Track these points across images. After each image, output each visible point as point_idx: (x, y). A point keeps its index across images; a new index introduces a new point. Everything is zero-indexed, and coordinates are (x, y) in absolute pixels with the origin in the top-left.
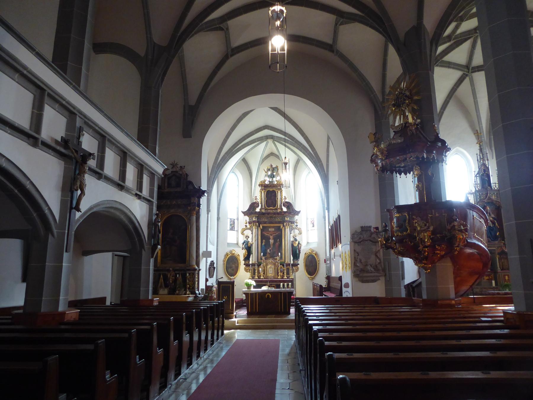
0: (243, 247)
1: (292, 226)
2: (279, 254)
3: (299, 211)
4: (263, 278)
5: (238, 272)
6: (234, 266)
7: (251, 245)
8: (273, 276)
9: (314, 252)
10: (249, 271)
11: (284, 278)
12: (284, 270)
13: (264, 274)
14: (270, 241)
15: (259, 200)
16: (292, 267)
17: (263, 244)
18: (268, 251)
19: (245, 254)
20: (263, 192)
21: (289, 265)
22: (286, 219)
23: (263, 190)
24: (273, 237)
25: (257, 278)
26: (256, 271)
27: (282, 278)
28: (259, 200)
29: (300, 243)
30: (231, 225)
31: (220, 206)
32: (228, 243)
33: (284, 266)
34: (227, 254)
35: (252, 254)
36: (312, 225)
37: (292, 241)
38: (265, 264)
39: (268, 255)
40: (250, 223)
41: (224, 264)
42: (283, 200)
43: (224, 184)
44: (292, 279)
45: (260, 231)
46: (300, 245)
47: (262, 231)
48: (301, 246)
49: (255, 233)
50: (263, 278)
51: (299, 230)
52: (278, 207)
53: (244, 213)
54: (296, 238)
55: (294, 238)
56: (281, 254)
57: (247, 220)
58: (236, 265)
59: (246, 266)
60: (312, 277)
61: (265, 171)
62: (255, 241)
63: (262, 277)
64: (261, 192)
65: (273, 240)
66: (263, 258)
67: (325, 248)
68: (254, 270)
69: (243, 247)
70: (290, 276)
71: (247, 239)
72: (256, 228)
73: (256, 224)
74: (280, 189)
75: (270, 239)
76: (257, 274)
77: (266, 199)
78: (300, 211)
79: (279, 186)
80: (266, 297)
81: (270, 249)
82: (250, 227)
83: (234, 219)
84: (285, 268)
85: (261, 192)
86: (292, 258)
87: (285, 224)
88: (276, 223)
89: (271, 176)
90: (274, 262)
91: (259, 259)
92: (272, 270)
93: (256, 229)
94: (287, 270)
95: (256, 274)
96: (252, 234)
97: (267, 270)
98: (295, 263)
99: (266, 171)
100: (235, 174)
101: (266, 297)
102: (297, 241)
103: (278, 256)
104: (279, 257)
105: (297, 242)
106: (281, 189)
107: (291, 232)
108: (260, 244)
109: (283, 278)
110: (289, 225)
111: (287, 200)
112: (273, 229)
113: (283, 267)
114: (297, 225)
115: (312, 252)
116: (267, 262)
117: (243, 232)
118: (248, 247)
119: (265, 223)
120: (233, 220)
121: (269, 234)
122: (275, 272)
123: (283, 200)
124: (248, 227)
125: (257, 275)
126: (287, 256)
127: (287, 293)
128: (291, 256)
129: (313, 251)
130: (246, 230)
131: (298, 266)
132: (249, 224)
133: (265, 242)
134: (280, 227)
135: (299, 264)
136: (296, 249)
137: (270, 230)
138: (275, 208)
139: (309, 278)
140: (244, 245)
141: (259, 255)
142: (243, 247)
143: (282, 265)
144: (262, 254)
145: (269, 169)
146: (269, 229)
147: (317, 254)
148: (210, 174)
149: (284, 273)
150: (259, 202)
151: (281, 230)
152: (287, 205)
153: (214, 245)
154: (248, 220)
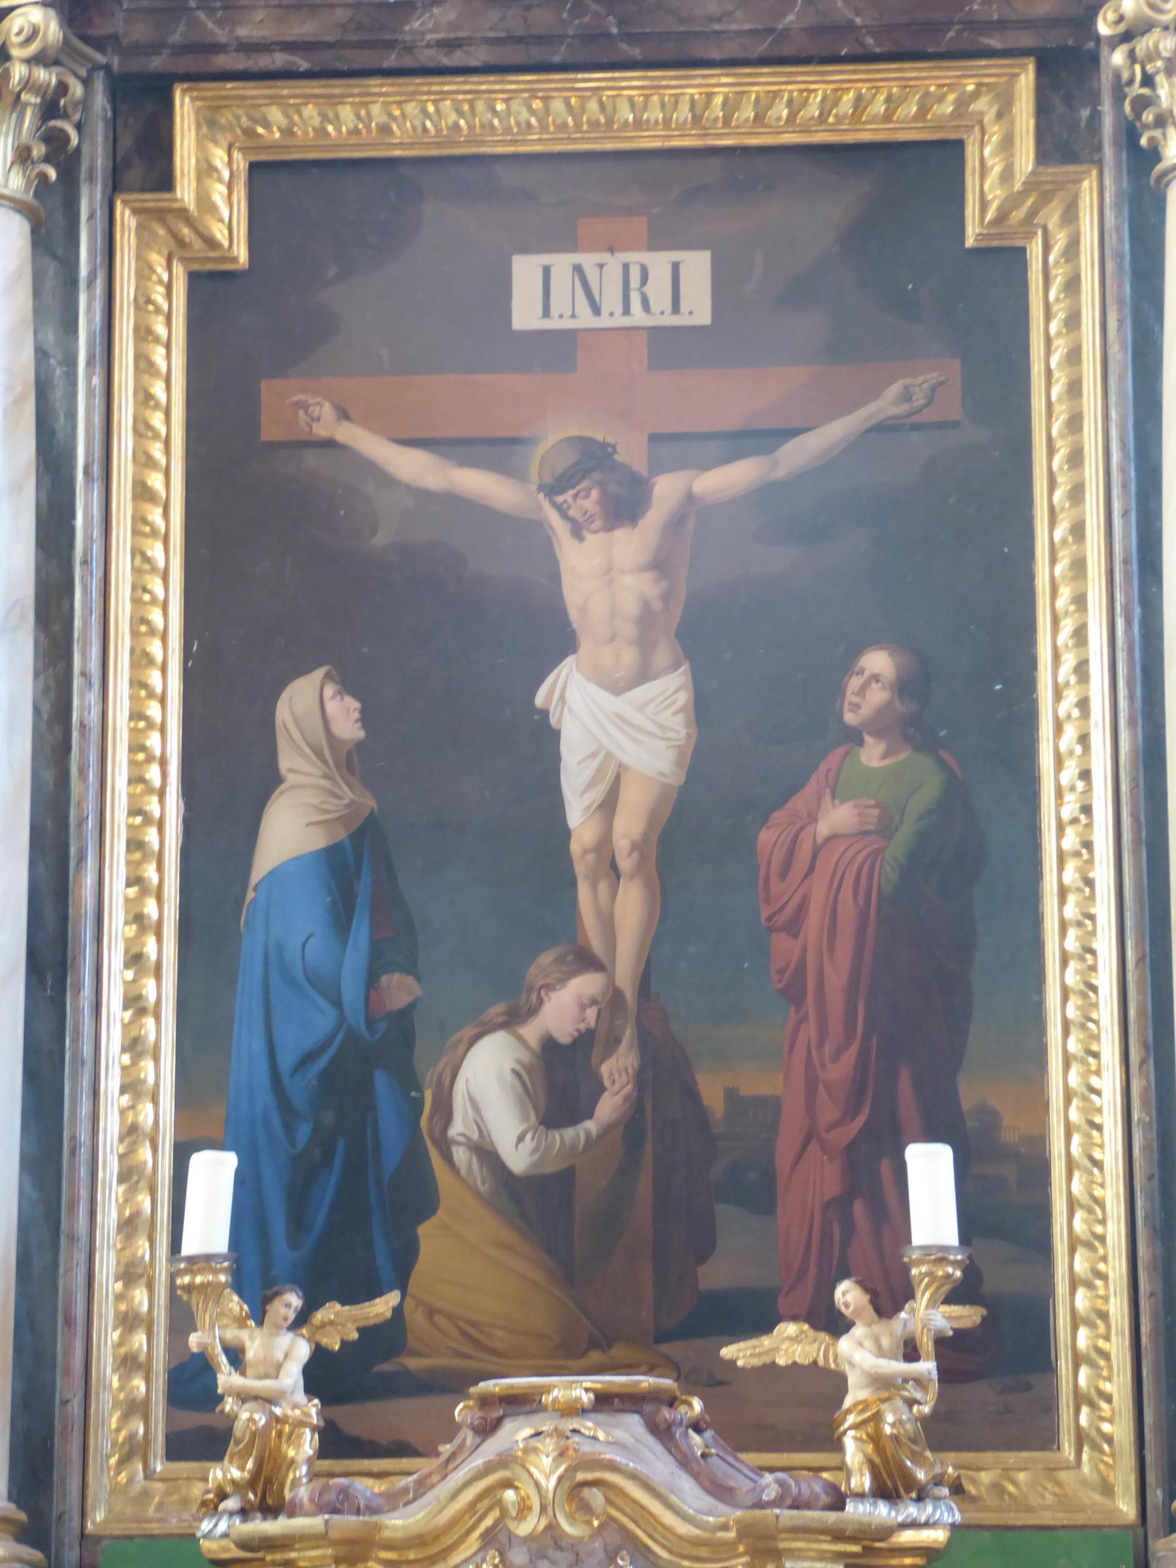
24: (659, 565)
116: (397, 1523)
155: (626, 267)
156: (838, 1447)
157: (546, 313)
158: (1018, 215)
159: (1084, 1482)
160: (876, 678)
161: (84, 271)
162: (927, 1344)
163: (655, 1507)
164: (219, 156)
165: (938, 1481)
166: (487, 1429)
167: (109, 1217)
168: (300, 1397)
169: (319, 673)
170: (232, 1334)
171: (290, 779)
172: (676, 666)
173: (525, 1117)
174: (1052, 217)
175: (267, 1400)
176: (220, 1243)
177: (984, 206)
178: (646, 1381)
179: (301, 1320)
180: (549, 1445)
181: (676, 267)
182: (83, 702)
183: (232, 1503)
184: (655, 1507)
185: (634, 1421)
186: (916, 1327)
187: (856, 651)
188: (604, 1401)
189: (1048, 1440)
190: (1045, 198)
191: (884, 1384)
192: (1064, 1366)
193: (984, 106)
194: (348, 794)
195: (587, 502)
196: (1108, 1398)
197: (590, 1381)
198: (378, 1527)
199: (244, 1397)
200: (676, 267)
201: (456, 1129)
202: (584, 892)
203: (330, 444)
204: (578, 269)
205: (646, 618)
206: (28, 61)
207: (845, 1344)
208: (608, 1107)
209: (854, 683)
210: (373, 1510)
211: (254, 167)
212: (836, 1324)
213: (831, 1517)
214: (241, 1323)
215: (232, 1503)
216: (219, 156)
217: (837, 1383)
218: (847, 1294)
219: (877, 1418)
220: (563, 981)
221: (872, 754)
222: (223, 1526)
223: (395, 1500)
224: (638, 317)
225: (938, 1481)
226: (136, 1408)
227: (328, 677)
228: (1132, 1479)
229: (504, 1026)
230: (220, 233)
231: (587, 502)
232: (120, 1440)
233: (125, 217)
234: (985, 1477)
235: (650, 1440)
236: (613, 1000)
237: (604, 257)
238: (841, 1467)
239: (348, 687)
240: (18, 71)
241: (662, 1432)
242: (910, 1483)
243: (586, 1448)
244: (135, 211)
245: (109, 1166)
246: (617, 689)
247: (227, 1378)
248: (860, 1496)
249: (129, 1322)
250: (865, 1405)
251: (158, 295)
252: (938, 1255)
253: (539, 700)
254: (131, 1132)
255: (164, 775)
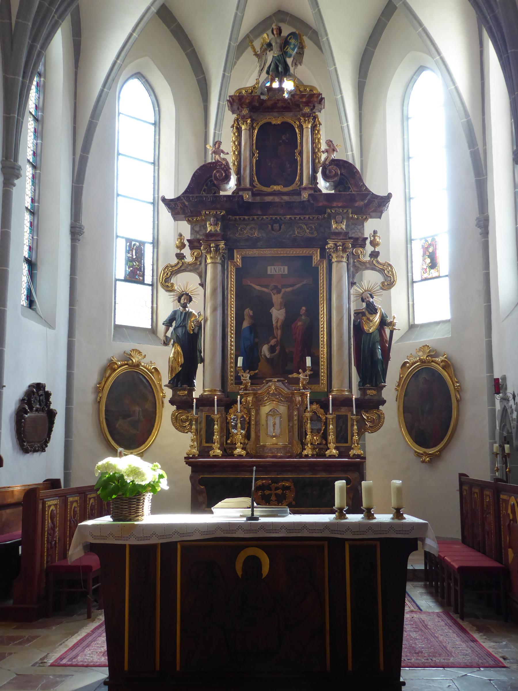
0: (169, 334)
1: (356, 256)
2: (308, 360)
3: (386, 195)
4: (244, 453)
5: (155, 432)
6: (137, 409)
7: (200, 327)
8: (285, 447)
9: (439, 360)
10: (191, 424)
11: (328, 453)
12: (326, 424)
13: (247, 436)
14: (271, 315)
15: (231, 159)
16: (358, 413)
17: (246, 324)
18: (265, 349)
19: (175, 359)
20: (243, 127)
21: (346, 402)
22: (334, 226)
23: (244, 118)
24: (282, 298)
25: (219, 452)
26: (216, 427)
27: (319, 456)
28: (231, 159)
29: (389, 320)
30: (129, 261)
31: (84, 186)
32: (118, 327)
33: (325, 406)
34: (111, 366)
35: (202, 361)
36: (428, 261)
37: (357, 313)
38: (250, 399)
39: (263, 366)
40: (194, 244)
41: (99, 402)
42: (323, 156)
43: (100, 95)
44: (358, 456)
45: (234, 277)
46: (387, 331)
47: (240, 273)
48: (392, 333)
49: (214, 278)
50: (244, 453)
51: (381, 271)
52: (302, 183)
53: (170, 204)
54: (371, 300)
55: (363, 300)
56: (316, 362)
57: (183, 235)
58: (148, 406)
59: (178, 408)
60: (431, 451)
61: (254, 51)
62: (214, 310)
63: (238, 451)
64: (239, 130)
65: (283, 311)
66: (246, 377)
67: (485, 340)
68: (210, 422)
69: (166, 337)
70: (350, 448)
71: (184, 306)
72: (219, 260)
73: (217, 246)
74: (309, 117)
75: (272, 305)
76: (221, 437)
77: (256, 155)
78: (389, 196)
79: (307, 104)
80: (240, 573)
81: (273, 342)
82: (196, 258)
83: (142, 243)
84: (329, 416)
85: (239, 130)
86: (355, 379)
87: (331, 244)
88: (295, 243)
89: (277, 67)
90: (285, 391)
91: (230, 382)
92: (277, 421)
93: (219, 267)
94: (337, 423)
95: (216, 437)
96: (203, 285)
97: (257, 423)
98: (367, 397)
99: (258, 49)
100: (147, 81)
101: (240, 573)
102: (376, 313)
103: (304, 370)
104: (308, 372)
105: (377, 319)
106: (315, 118)
107: (353, 278)
108: (234, 325)
109: (324, 456)
110: (344, 250)
111: (335, 156)
112: (284, 270)
113: (322, 411)
114: (378, 253)
115: (432, 356)
116: (259, 392)
117: (167, 280)
118: (187, 333)
119: (253, 244)
120: (138, 244)
121: (266, 286)
122: (291, 430)
123: (323, 156)
124: (189, 259)
125: (222, 445)
126: (341, 371)
127: (378, 543)
128: (354, 369)
129: (433, 354)
130: (178, 271)
131: (381, 407)
132: (192, 248)
133: (252, 317)
134: (310, 258)
135: (383, 402)
136: (374, 344)
137: (271, 270)
138: (290, 188)
139: (419, 455)
140: (171, 329)
141: (230, 360)
142: (166, 337)
143: (318, 402)
144: (240, 360)
145: (269, 45)
146: (269, 268)
147: (452, 364)
148: (18, 17)
149: (325, 436)
150: (231, 165)
151: (314, 273)
152: (336, 174)
153: (50, 324)
154: (187, 235)
155: (279, 268)
156: (299, 384)
157: (271, 272)
158: (318, 263)
159: (322, 388)
160: (304, 310)
161: (226, 268)
162: (308, 375)
163: (283, 391)
164: (238, 256)
165: (309, 388)
166: (267, 383)
167: (229, 362)
168: (249, 380)
169: (248, 308)
170: (242, 374)
171: (246, 319)
172: (284, 308)
173: (269, 352)
174: (321, 264)
175: (246, 380)
176: (241, 365)
177: (315, 262)
178: (282, 379)
179: (249, 373)
180: (273, 385)
181: (284, 268)
182: (226, 312)
183: (243, 389)
184: (283, 391)
185: (281, 383)
186: (307, 374)
187: (302, 307)
188: (278, 381)
189: (319, 384)
190: (320, 262)
191: (304, 379)
192: (320, 377)
193: (315, 252)
194: (251, 321)
195: (275, 291)
196: (324, 380)
197: (277, 379)
198: (257, 392)
199: (244, 380)
200: (284, 268)
201: (262, 354)
202: (275, 331)
203: (250, 285)
204: (274, 268)
205: (281, 303)
206: (222, 250)
207: (300, 375)
208: (277, 352)
209: (301, 310)
210: (257, 391)
211: (242, 257)
212: (299, 373)
213: (299, 391)
214: (243, 373)
215: (243, 389)
216: (238, 256)
217: (299, 379)
218: (300, 371)
219: (303, 382)
220: (272, 340)
221: (303, 317)
222: (242, 391)
223: (259, 389)
224: (280, 273)
225: (309, 388)
226: (232, 380)
227: (249, 309)
228: (327, 387)
229: (267, 344)
230: (238, 264)
231: (275, 291)
232: (510, 550)
233: (229, 262)
234: (313, 387)
235: (282, 385)
236: (277, 341)
237: (277, 267)
238: (300, 386)
239: (251, 310)
240: (221, 251)
241: (283, 384)
242: (306, 388)
243: (277, 385)
244: (230, 262)
245: (229, 357)
246: (278, 310)
247: (242, 378)
248: (301, 389)
249: (231, 372)
250: (302, 381)
251: (232, 270)
252: (309, 367)
253: (270, 312)
254: (231, 353)
255: (233, 319)
